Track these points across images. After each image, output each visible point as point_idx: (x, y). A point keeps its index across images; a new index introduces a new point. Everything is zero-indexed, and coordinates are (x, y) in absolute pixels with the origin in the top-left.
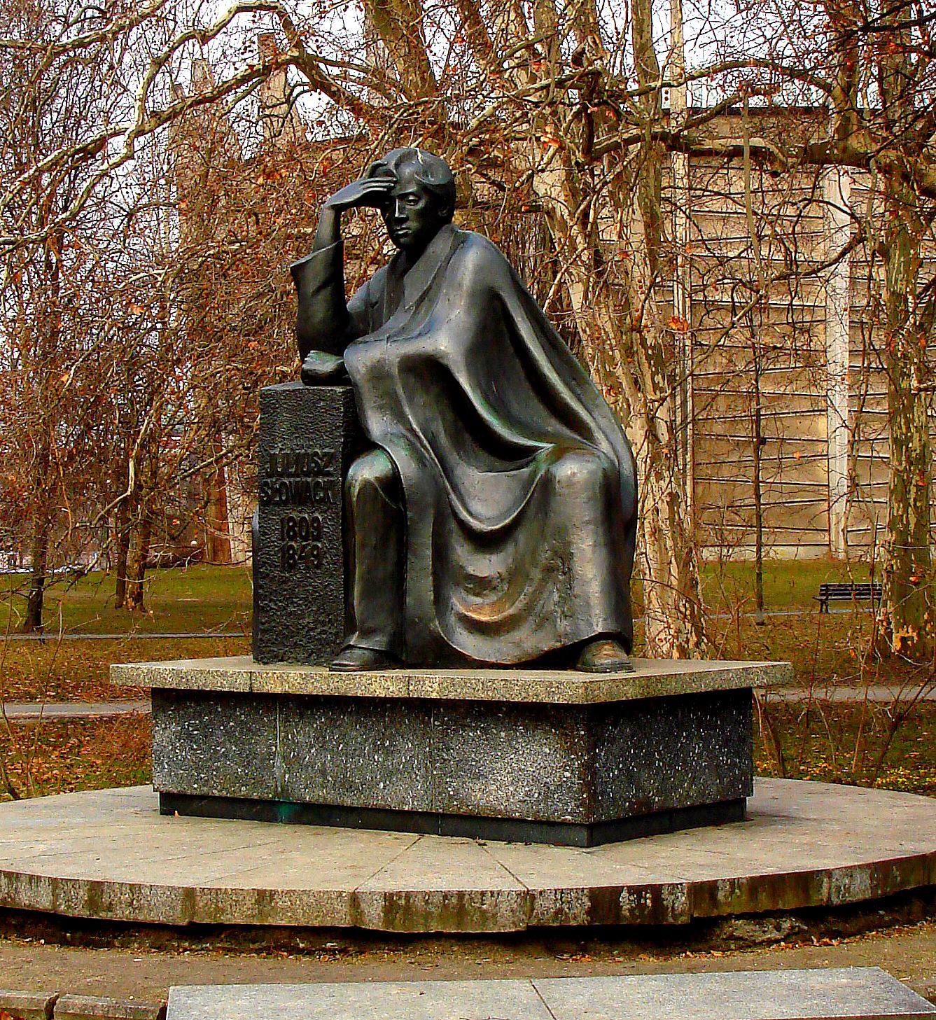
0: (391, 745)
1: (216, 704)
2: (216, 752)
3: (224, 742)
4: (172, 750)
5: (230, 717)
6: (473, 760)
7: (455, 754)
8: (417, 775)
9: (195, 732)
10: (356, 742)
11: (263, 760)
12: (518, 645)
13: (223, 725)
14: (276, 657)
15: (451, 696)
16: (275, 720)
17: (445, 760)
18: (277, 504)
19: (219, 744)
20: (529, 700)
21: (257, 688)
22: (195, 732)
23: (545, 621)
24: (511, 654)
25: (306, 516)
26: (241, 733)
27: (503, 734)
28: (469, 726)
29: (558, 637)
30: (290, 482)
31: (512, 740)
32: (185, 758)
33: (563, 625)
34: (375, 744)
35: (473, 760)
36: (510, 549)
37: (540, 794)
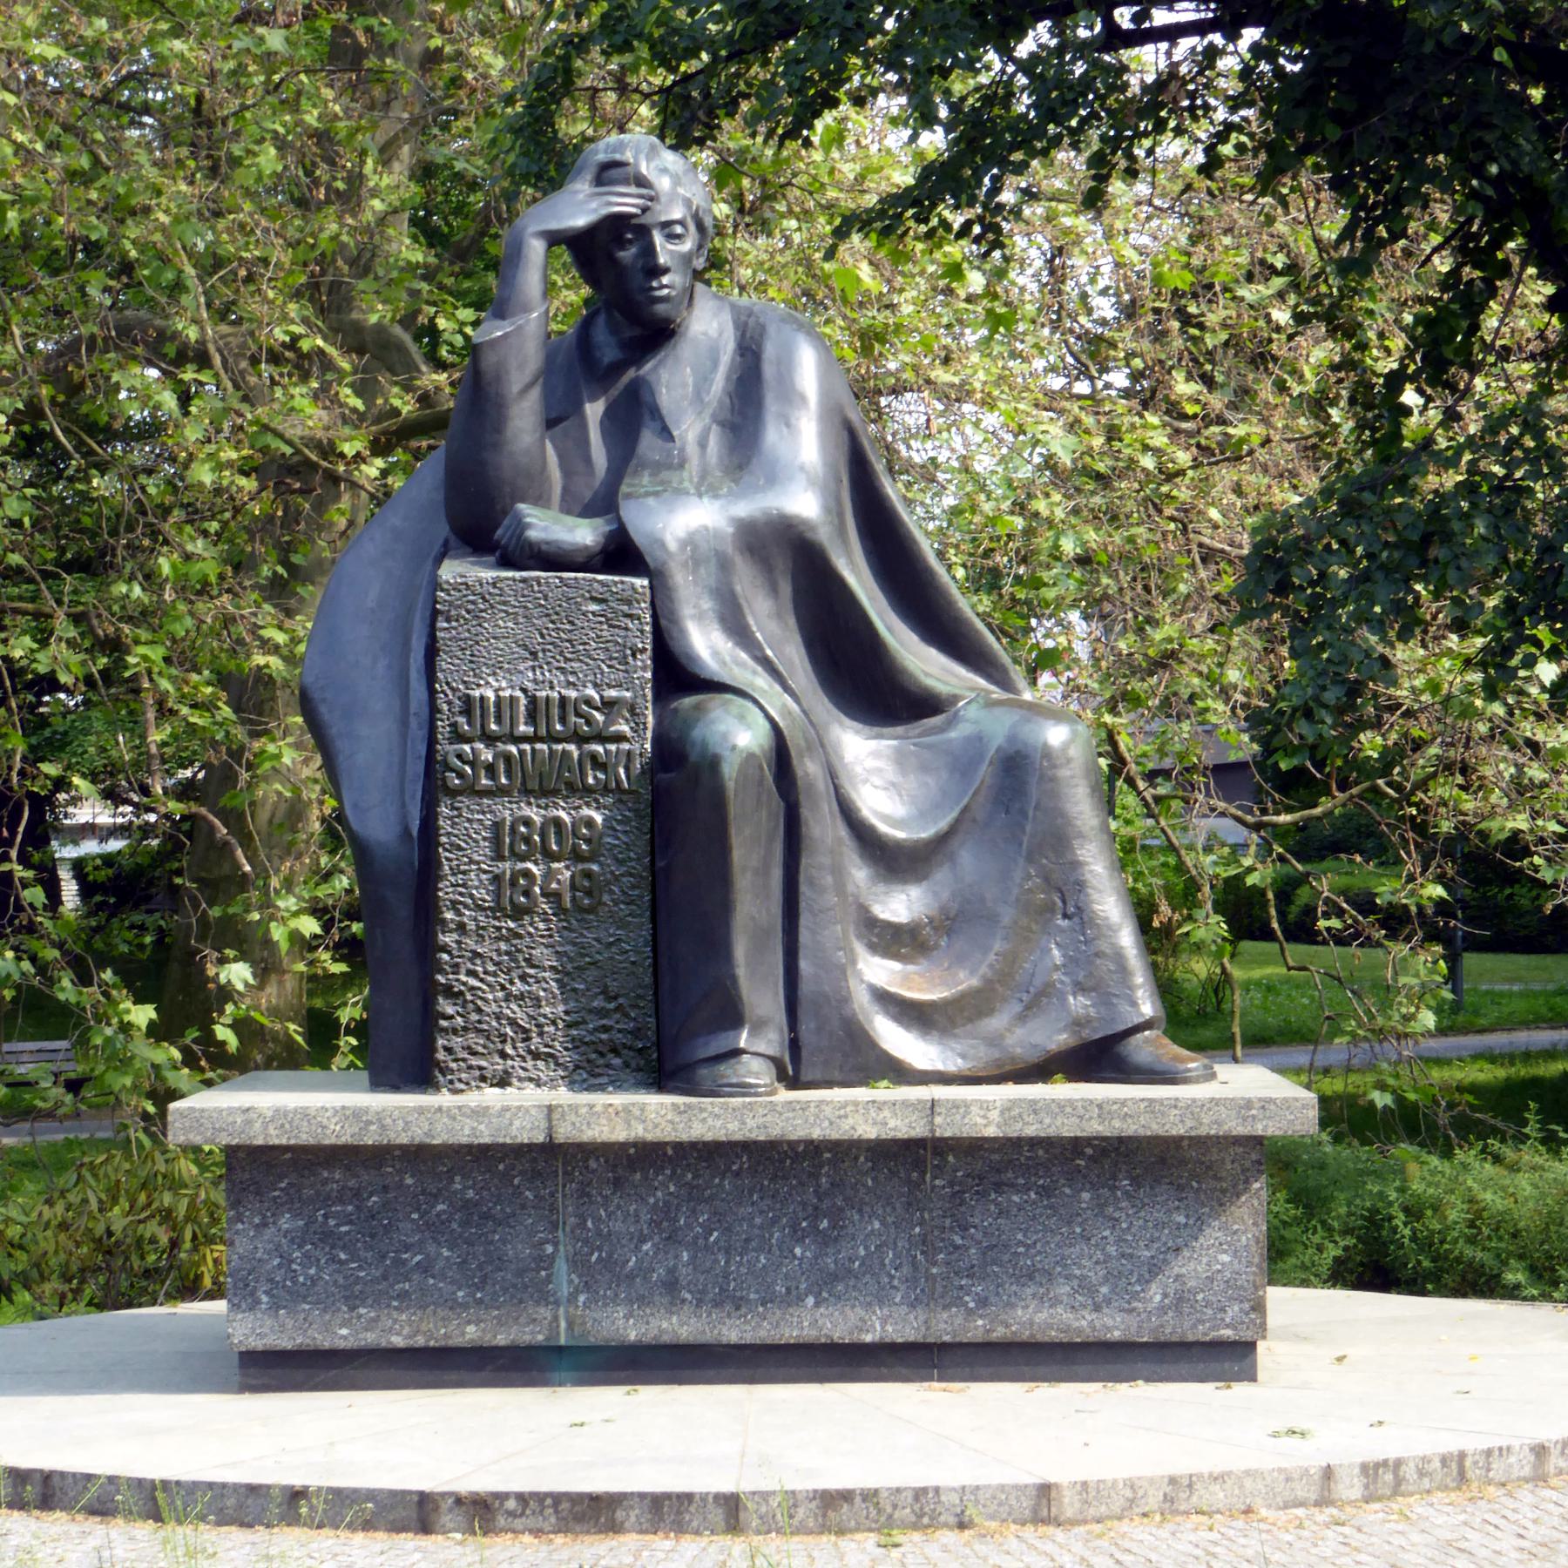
0: (833, 1226)
1: (400, 1172)
2: (399, 1262)
3: (421, 1242)
4: (280, 1266)
5: (435, 1196)
6: (1020, 1243)
7: (979, 1236)
8: (892, 1277)
9: (344, 1229)
10: (752, 1226)
11: (520, 1273)
12: (994, 1041)
13: (418, 1210)
14: (483, 1079)
15: (1030, 1131)
16: (552, 1195)
17: (957, 1248)
18: (487, 793)
19: (407, 1248)
20: (1203, 1131)
21: (564, 1133)
22: (344, 1229)
23: (1038, 1000)
24: (953, 1064)
25: (563, 814)
26: (465, 1224)
27: (1086, 1196)
28: (1012, 1185)
29: (1078, 1023)
30: (522, 753)
31: (1106, 1205)
32: (314, 1281)
33: (1078, 1004)
34: (795, 1227)
35: (1020, 1243)
36: (942, 875)
37: (1165, 1295)
